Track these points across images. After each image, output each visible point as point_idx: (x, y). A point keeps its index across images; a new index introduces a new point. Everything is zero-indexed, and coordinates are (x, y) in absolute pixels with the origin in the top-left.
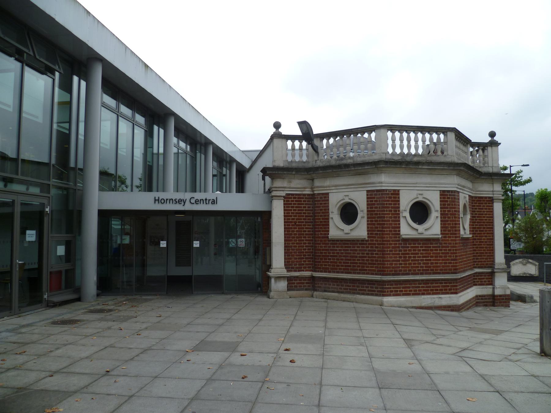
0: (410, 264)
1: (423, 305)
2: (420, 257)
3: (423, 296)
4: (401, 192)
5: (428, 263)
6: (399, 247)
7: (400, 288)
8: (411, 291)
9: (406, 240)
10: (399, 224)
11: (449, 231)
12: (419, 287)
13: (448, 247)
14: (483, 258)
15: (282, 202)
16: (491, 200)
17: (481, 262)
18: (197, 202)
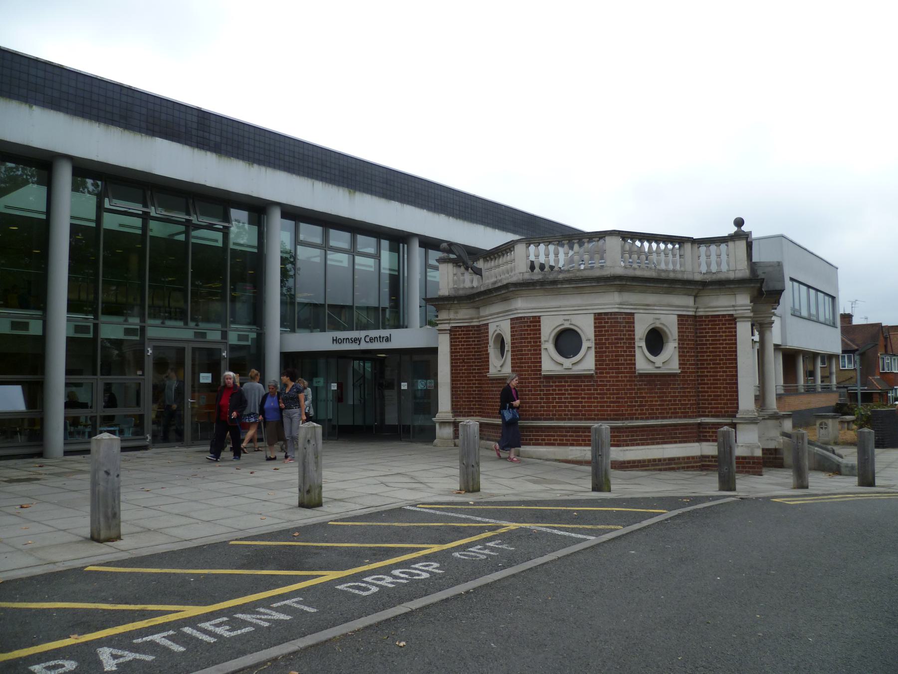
0: (555, 407)
1: (570, 458)
2: (567, 398)
3: (571, 448)
4: (542, 319)
5: (578, 407)
6: (540, 386)
7: (541, 436)
8: (556, 440)
9: (549, 378)
10: (540, 358)
11: (607, 365)
12: (566, 436)
13: (606, 385)
14: (720, 404)
15: (448, 336)
16: (732, 320)
17: (717, 408)
18: (372, 340)
